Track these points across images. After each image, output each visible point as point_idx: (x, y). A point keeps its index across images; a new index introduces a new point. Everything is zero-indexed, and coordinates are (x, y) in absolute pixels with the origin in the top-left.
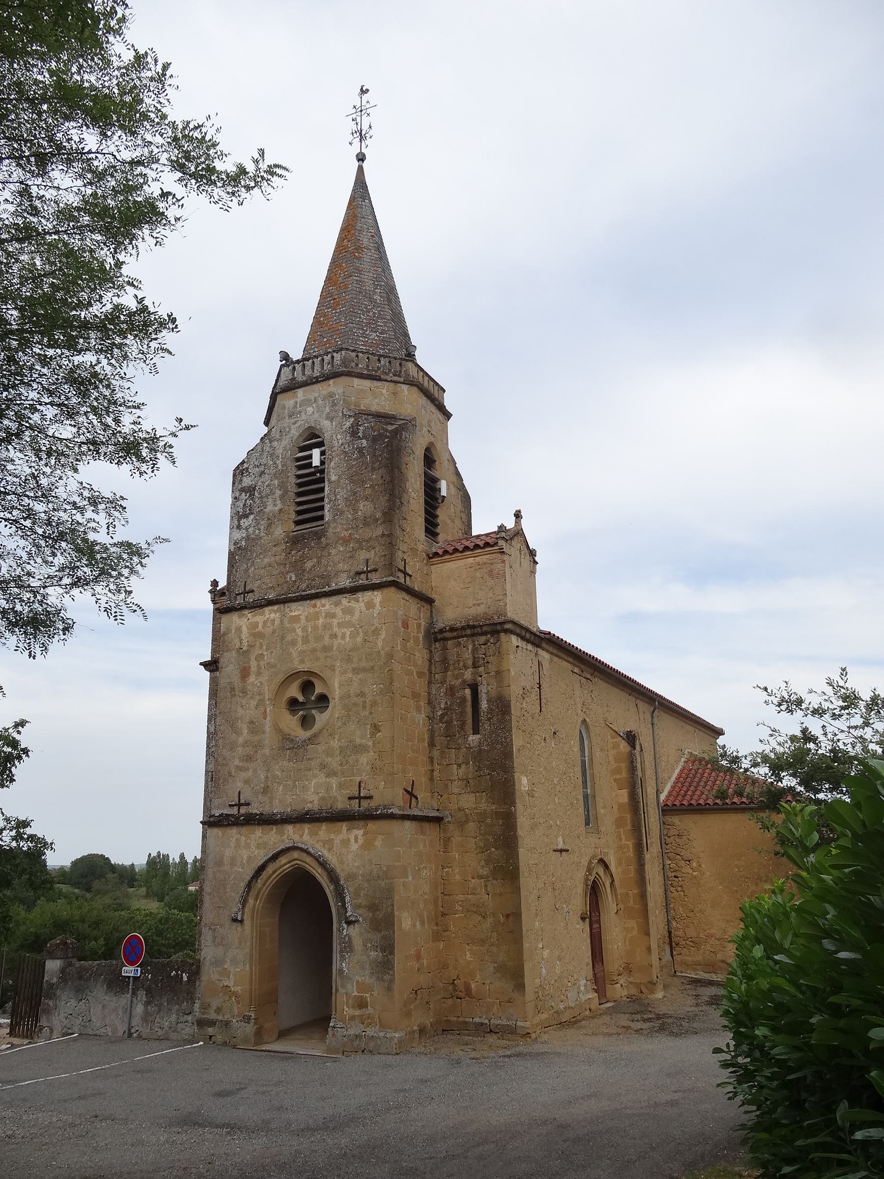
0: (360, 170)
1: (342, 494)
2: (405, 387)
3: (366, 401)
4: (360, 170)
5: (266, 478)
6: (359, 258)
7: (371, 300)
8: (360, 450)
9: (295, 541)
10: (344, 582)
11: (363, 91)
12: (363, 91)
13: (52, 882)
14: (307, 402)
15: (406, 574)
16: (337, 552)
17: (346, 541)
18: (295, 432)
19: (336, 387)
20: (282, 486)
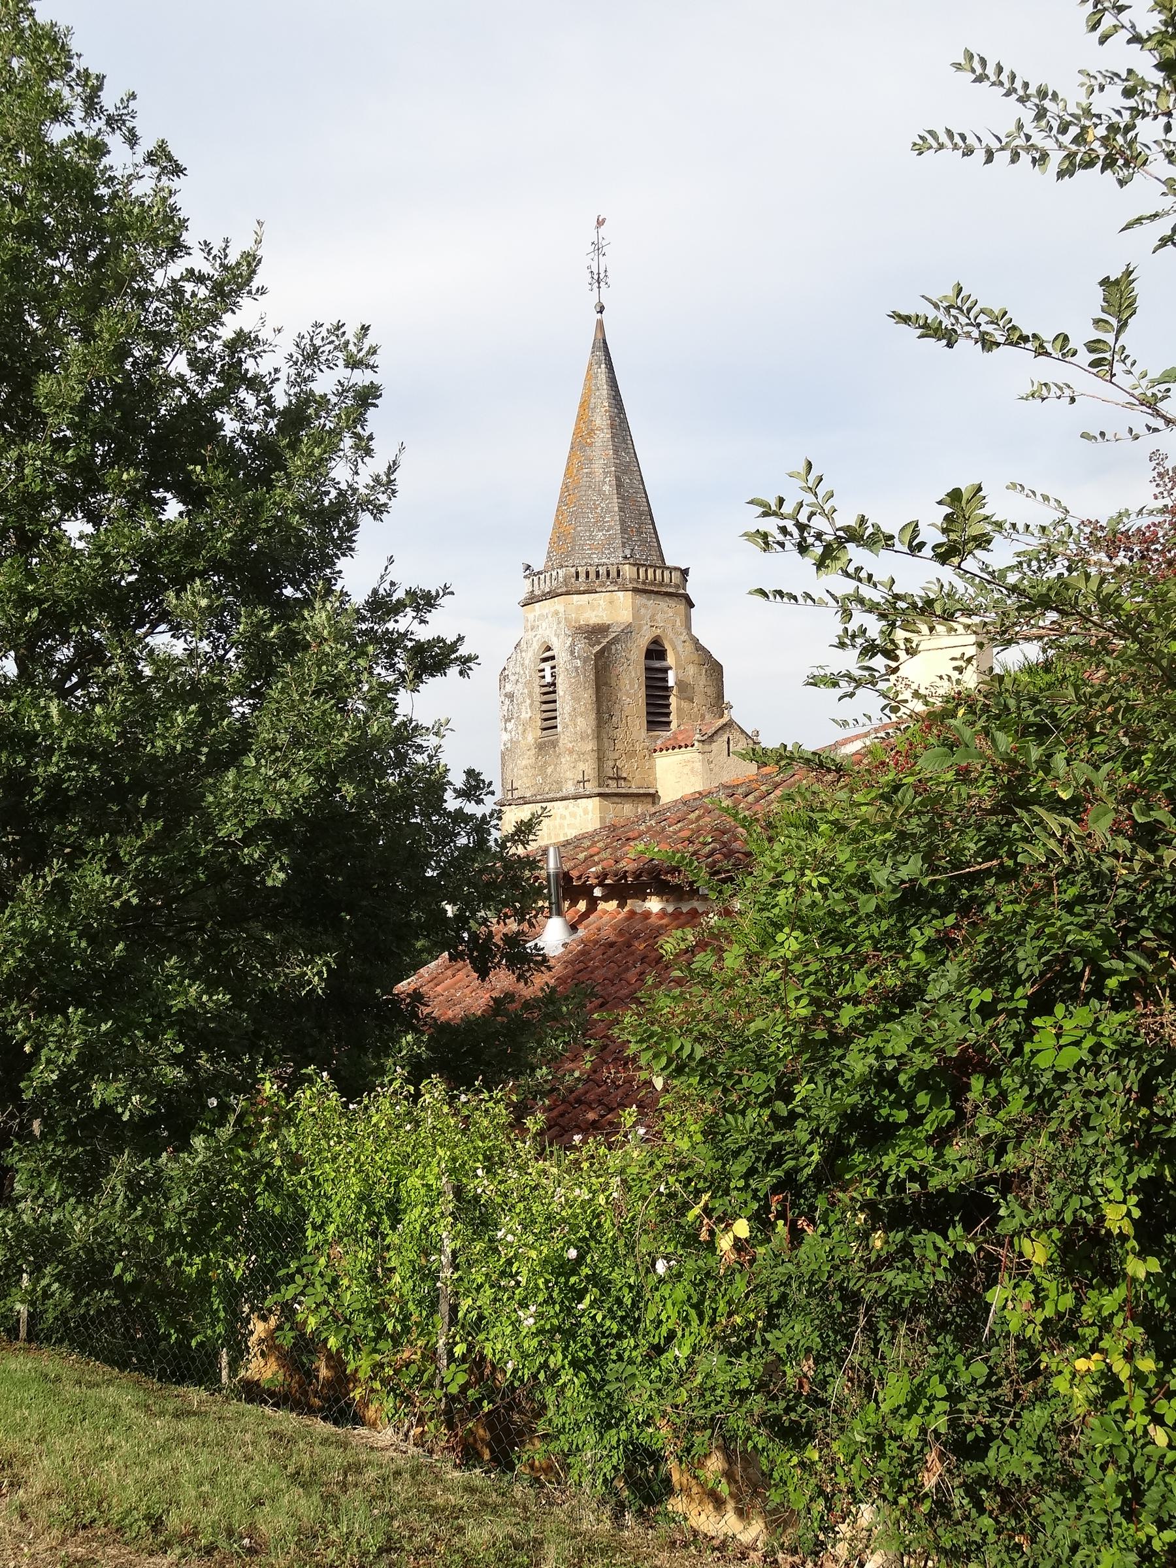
0: (600, 325)
1: (567, 709)
2: (620, 594)
3: (586, 615)
4: (600, 325)
5: (520, 686)
6: (591, 445)
7: (600, 492)
8: (577, 668)
9: (541, 747)
10: (570, 788)
11: (600, 223)
12: (600, 223)
13: (65, 510)
14: (543, 617)
15: (618, 778)
16: (566, 760)
17: (571, 752)
18: (536, 646)
19: (557, 604)
20: (530, 695)
